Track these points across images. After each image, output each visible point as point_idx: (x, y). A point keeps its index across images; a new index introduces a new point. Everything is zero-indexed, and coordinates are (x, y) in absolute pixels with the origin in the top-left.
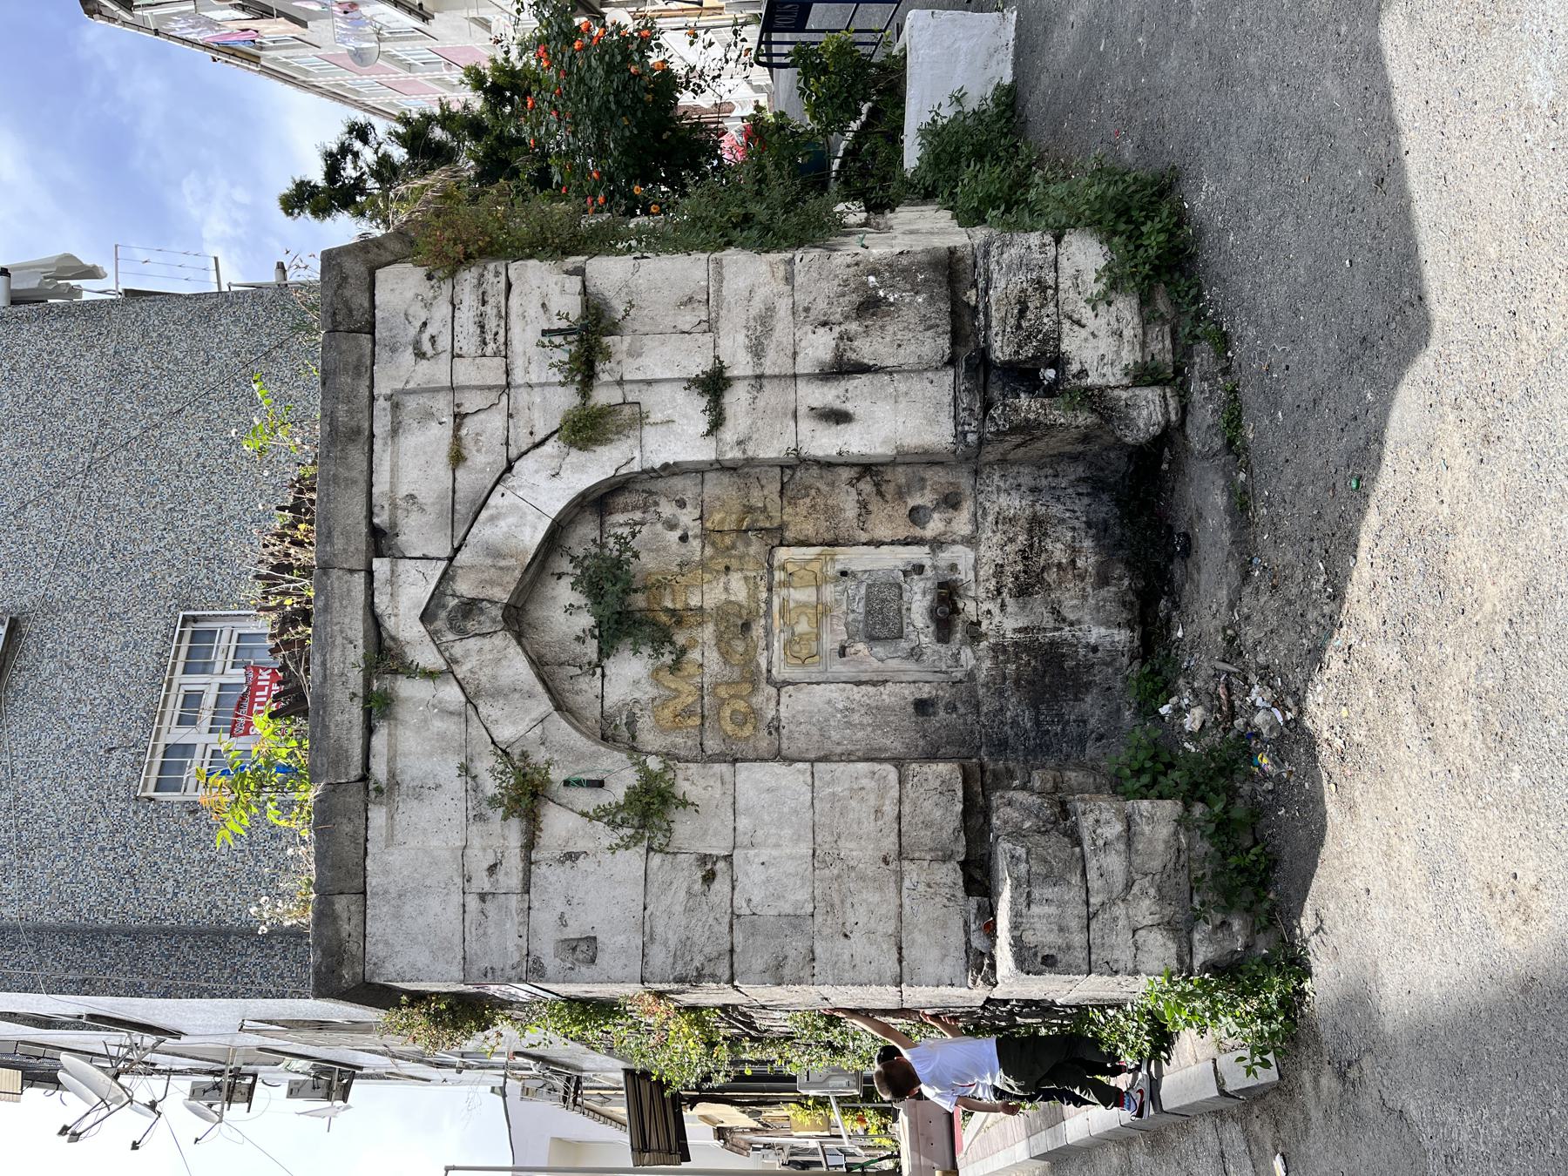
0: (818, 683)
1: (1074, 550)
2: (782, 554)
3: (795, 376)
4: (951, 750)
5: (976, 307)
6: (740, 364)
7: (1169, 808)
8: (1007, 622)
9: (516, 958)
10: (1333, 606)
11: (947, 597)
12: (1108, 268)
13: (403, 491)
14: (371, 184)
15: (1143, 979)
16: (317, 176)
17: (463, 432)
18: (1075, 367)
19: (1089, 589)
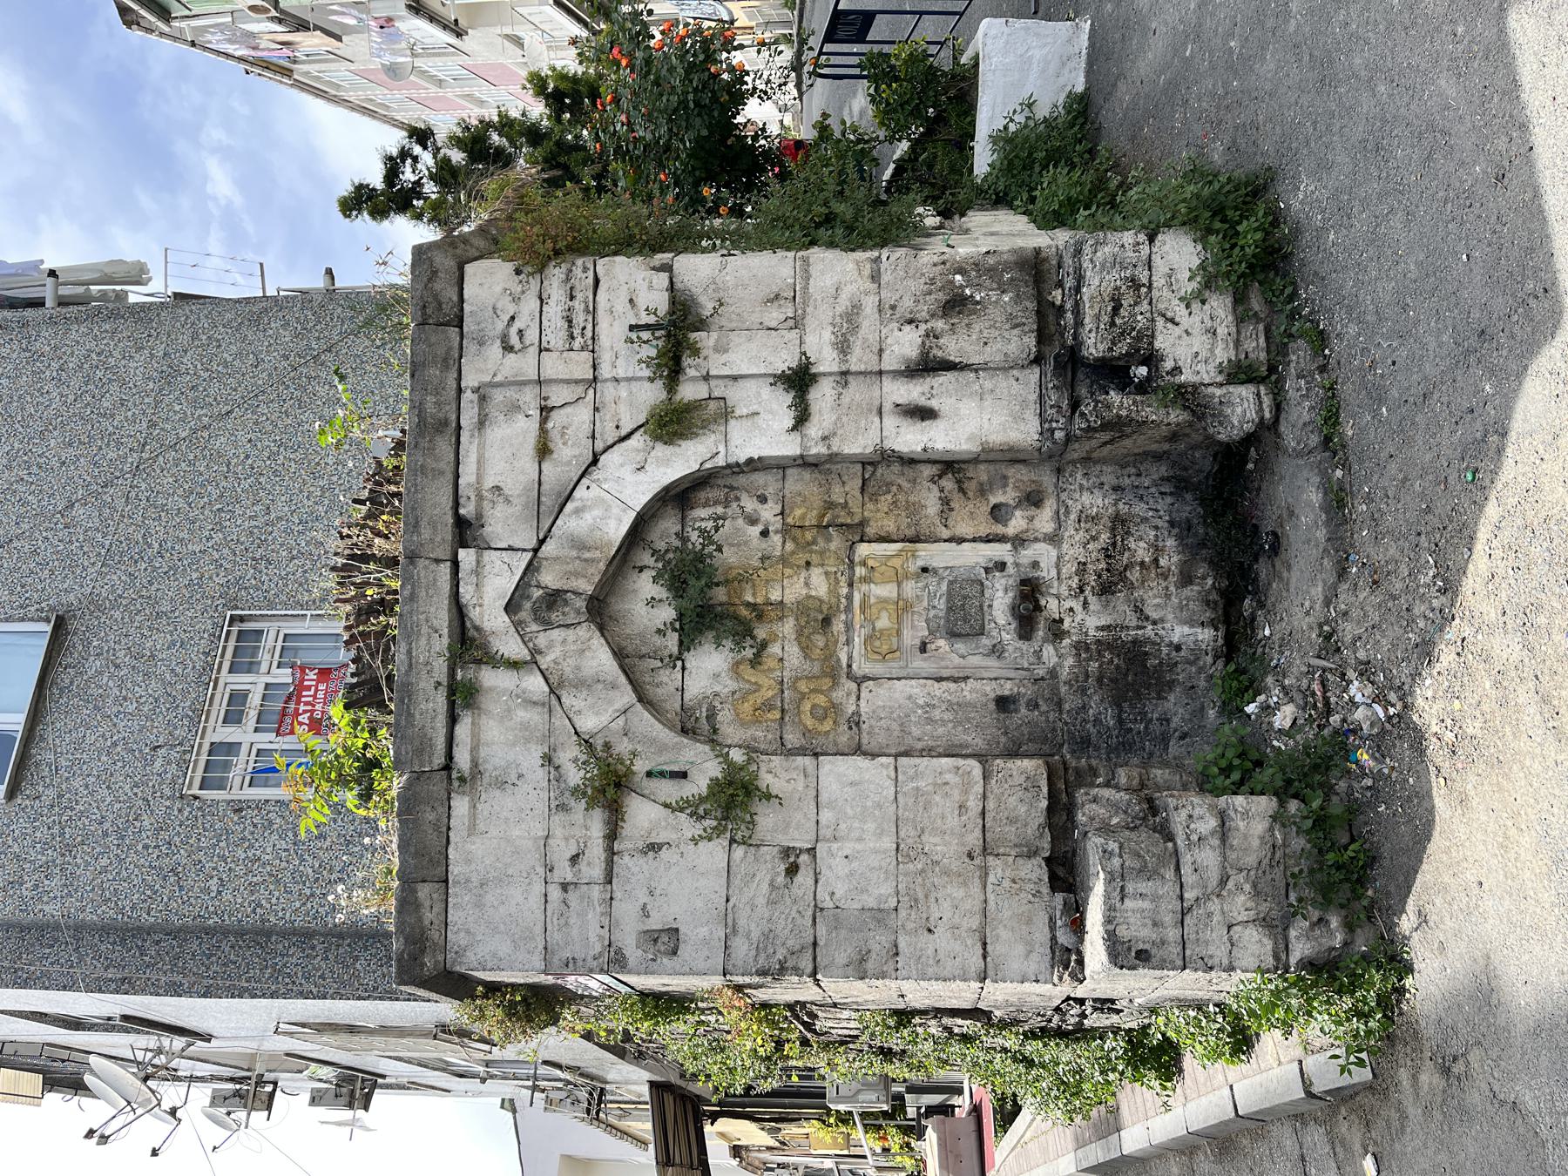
0: (899, 679)
1: (1157, 550)
2: (863, 550)
3: (881, 373)
4: (1032, 747)
5: (1062, 306)
6: (826, 360)
7: (1264, 804)
8: (1090, 620)
9: (598, 948)
10: (1443, 599)
11: (1029, 593)
12: (1202, 267)
13: (489, 483)
14: (430, 188)
15: (1238, 975)
16: (376, 180)
17: (550, 425)
18: (1168, 365)
19: (1172, 588)
